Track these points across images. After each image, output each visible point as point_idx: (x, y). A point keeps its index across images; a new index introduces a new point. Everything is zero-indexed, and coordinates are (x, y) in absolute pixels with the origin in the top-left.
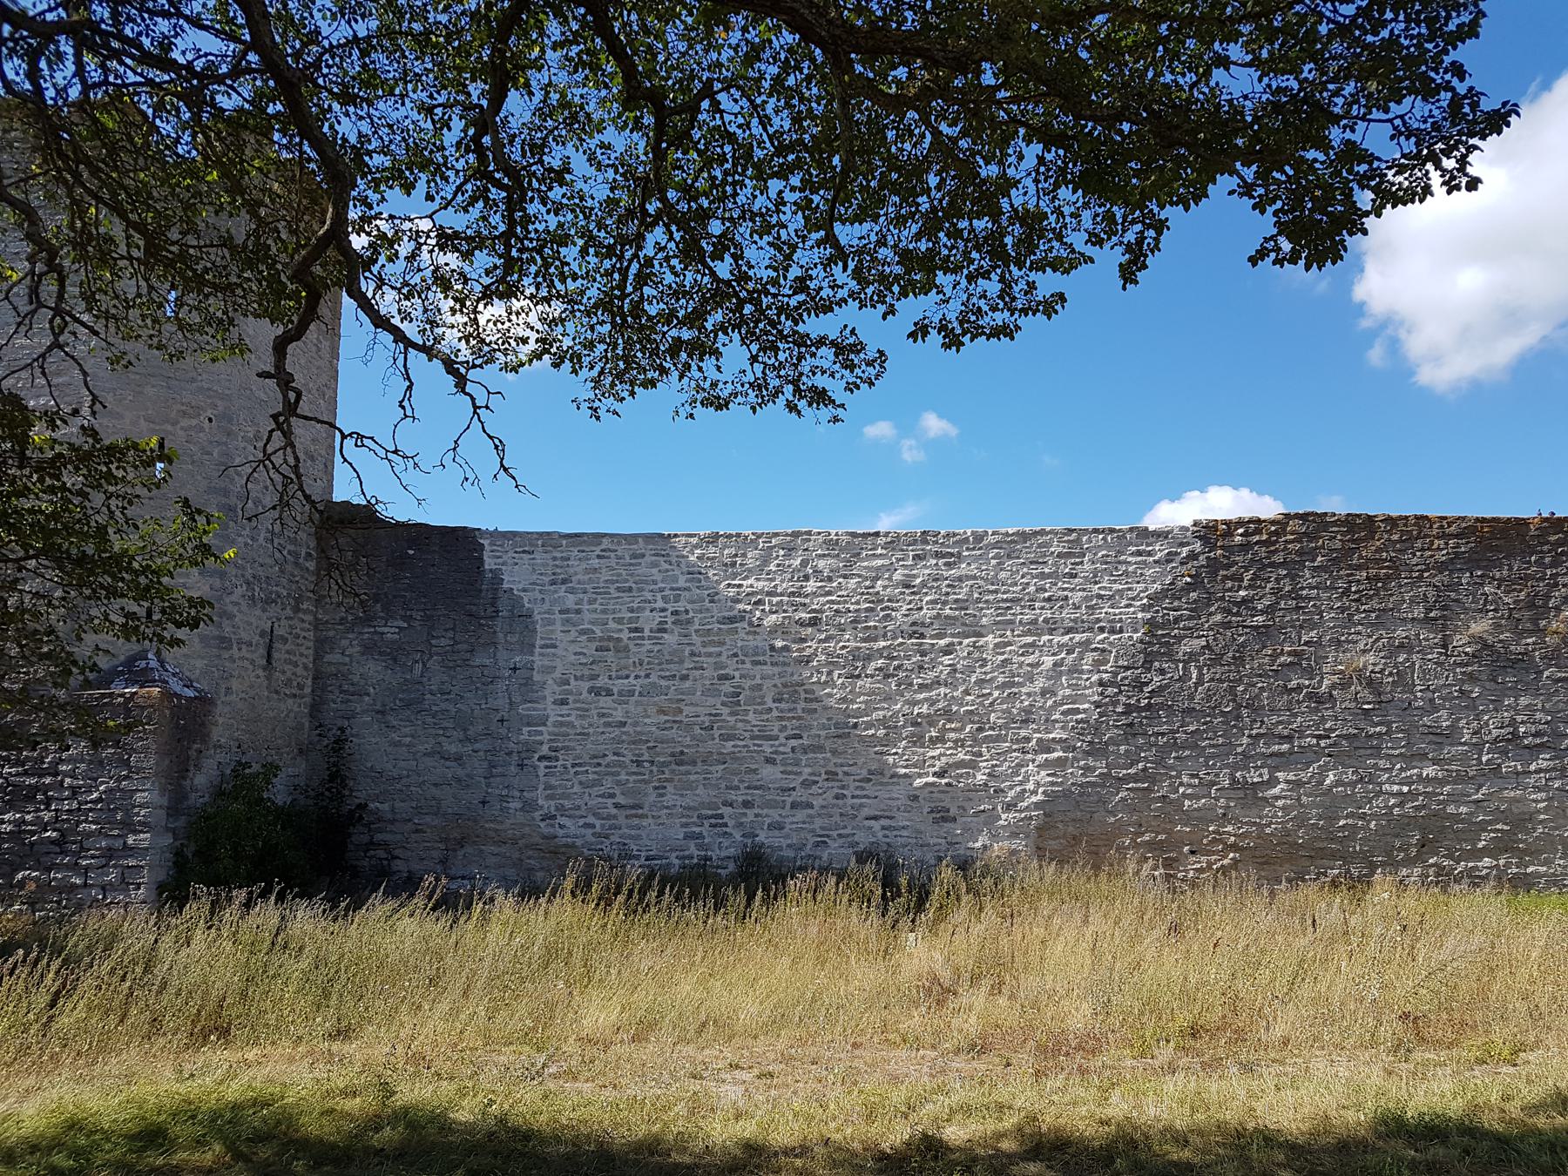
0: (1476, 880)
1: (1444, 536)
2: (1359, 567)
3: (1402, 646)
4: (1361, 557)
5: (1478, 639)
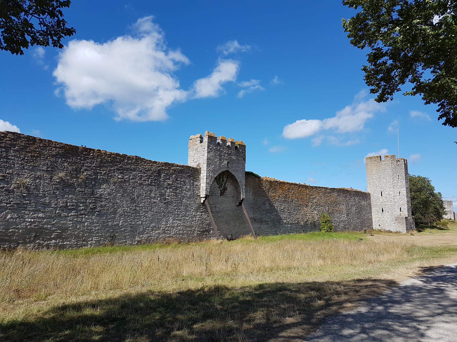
0: (48, 247)
1: (56, 147)
2: (29, 152)
3: (38, 177)
4: (30, 149)
5: (61, 178)
